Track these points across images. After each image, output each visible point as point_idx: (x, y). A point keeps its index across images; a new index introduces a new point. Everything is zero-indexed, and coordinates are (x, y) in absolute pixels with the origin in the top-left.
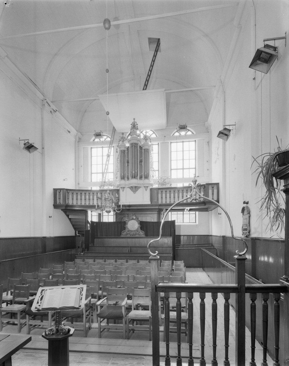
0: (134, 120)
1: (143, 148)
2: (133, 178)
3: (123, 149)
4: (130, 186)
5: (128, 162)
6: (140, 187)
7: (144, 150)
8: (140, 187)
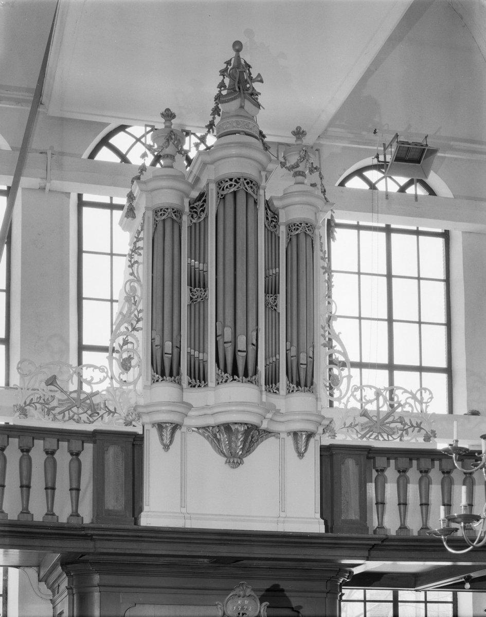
0: (238, 51)
1: (283, 219)
2: (235, 372)
3: (168, 198)
4: (211, 421)
5: (197, 282)
6: (268, 433)
7: (291, 227)
8: (268, 433)
